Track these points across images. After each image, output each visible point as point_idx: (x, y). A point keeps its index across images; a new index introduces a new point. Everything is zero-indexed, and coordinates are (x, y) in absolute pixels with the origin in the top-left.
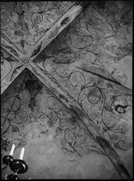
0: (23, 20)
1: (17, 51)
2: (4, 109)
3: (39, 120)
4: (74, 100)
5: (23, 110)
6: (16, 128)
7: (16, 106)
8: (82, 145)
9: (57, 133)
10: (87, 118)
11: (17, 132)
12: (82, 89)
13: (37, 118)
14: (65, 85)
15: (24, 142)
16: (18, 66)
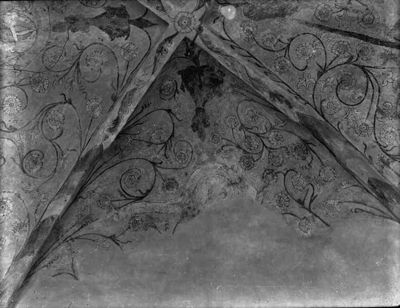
2: (140, 141)
3: (219, 158)
4: (304, 102)
5: (181, 139)
6: (171, 181)
8: (331, 202)
9: (265, 182)
10: (340, 140)
12: (320, 75)
13: (213, 153)
14: (279, 70)
15: (192, 208)
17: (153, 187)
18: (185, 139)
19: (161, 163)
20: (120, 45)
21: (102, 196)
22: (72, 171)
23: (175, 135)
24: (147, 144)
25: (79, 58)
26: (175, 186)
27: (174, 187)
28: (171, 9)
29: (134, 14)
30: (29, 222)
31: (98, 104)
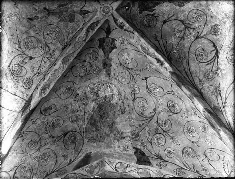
0: (55, 10)
1: (92, 22)
2: (178, 44)
11: (219, 27)
16: (114, 22)
18: (187, 13)
19: (198, 32)
20: (120, 45)
21: (206, 76)
23: (182, 20)
24: (182, 40)
25: (125, 67)
28: (98, 17)
29: (103, 35)
30: (203, 123)
31: (149, 65)
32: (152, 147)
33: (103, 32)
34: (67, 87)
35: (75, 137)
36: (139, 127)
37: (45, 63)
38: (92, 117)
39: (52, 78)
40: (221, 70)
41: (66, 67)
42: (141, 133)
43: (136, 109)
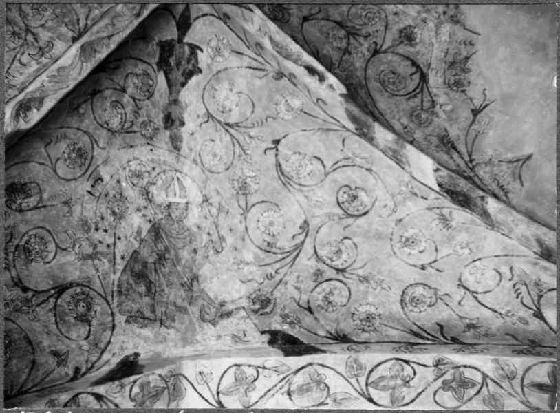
5: (346, 13)
6: (403, 35)
7: (333, 31)
11: (416, 30)
17: (408, 58)
20: (209, 61)
22: (373, 145)
25: (220, 122)
26: (412, 29)
27: (412, 32)
30: (438, 208)
31: (283, 102)
32: (316, 319)
33: (172, 25)
34: (77, 147)
35: (90, 304)
36: (266, 281)
37: (24, 65)
38: (135, 255)
39: (50, 85)
40: (441, 105)
41: (88, 67)
42: (277, 294)
43: (252, 237)
